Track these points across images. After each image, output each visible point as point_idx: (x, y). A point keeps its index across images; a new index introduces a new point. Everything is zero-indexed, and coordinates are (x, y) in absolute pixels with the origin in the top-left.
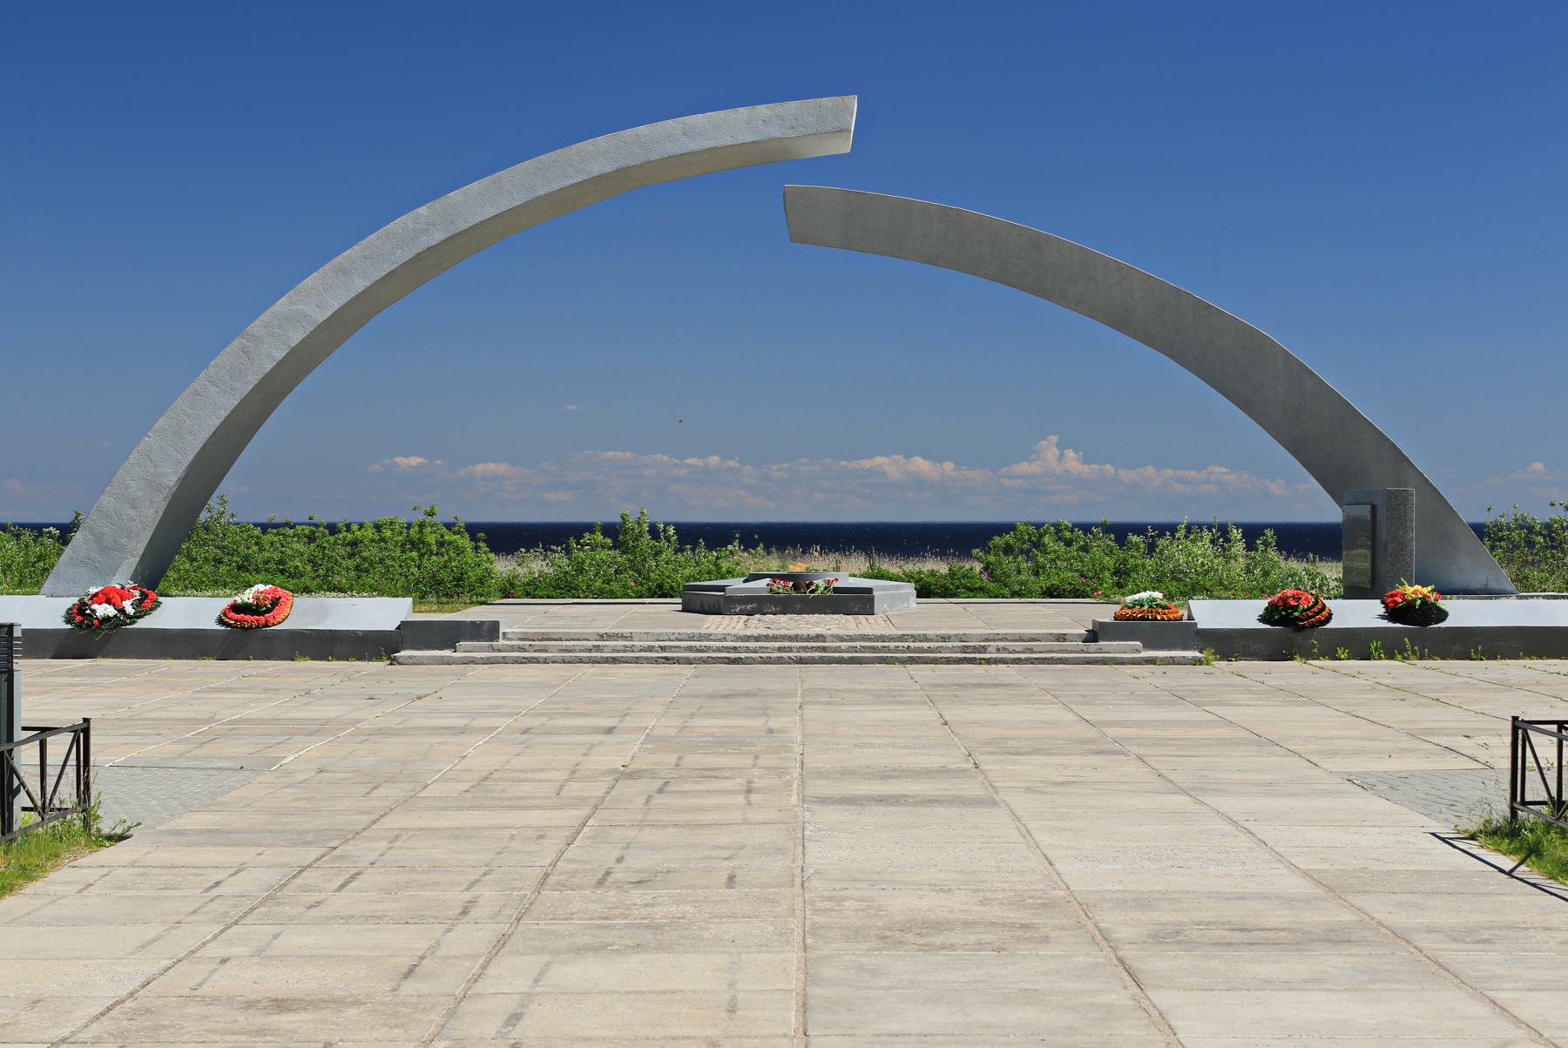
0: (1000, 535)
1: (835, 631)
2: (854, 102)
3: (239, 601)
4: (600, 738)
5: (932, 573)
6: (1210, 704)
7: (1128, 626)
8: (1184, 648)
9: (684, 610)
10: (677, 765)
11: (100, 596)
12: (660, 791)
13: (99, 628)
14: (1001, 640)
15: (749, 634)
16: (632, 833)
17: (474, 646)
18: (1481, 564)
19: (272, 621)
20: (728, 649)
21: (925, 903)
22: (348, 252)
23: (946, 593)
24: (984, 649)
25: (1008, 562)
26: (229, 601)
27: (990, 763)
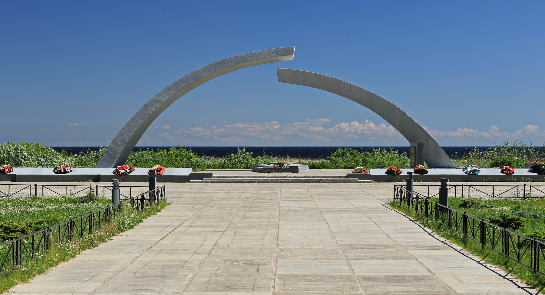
1: (289, 176)
9: (253, 172)
12: (255, 199)
13: (121, 175)
16: (253, 203)
20: (264, 180)
24: (322, 180)
27: (314, 197)
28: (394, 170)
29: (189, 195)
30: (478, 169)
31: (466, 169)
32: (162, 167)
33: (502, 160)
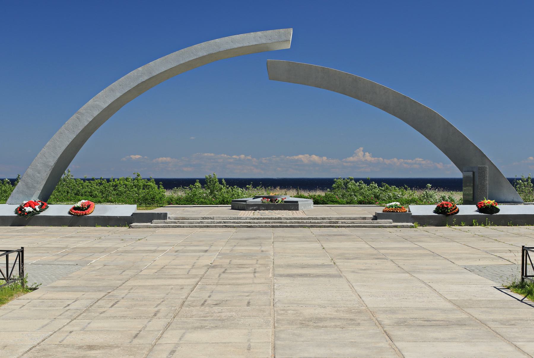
1: (285, 216)
2: (291, 31)
3: (76, 206)
5: (319, 196)
7: (387, 214)
8: (407, 222)
9: (231, 209)
10: (230, 263)
11: (27, 204)
12: (224, 272)
14: (343, 219)
15: (255, 217)
16: (214, 287)
20: (247, 223)
21: (316, 312)
24: (337, 223)
26: (73, 206)
27: (339, 262)
28: (448, 207)
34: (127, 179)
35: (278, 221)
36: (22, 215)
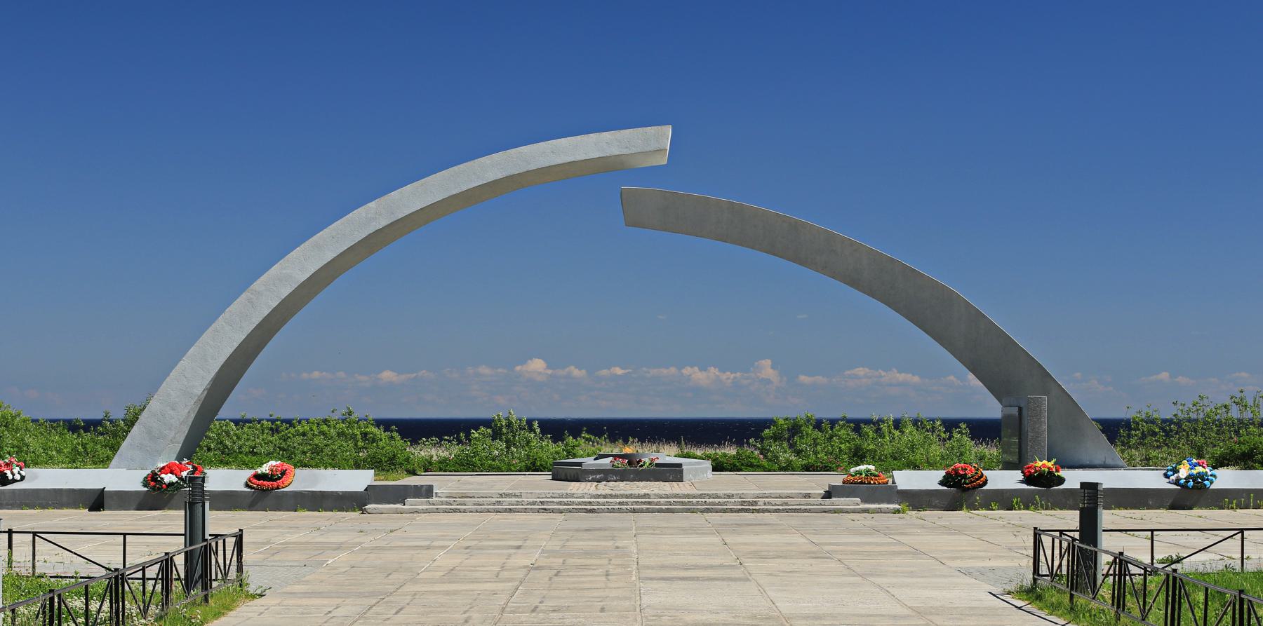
0: (769, 428)
1: (656, 491)
2: (668, 130)
3: (260, 472)
4: (514, 551)
5: (725, 455)
6: (891, 534)
7: (851, 488)
8: (888, 503)
10: (563, 564)
11: (166, 468)
12: (556, 575)
14: (767, 497)
15: (599, 493)
16: (545, 592)
17: (416, 501)
18: (1100, 447)
19: (281, 485)
20: (586, 504)
21: (704, 618)
22: (321, 233)
23: (734, 468)
24: (756, 503)
25: (775, 447)
26: (252, 472)
27: (749, 563)
28: (966, 474)
29: (343, 556)
30: (1209, 473)
31: (1175, 471)
32: (286, 466)
33: (1245, 448)
34: (326, 421)
35: (643, 500)
36: (156, 488)
